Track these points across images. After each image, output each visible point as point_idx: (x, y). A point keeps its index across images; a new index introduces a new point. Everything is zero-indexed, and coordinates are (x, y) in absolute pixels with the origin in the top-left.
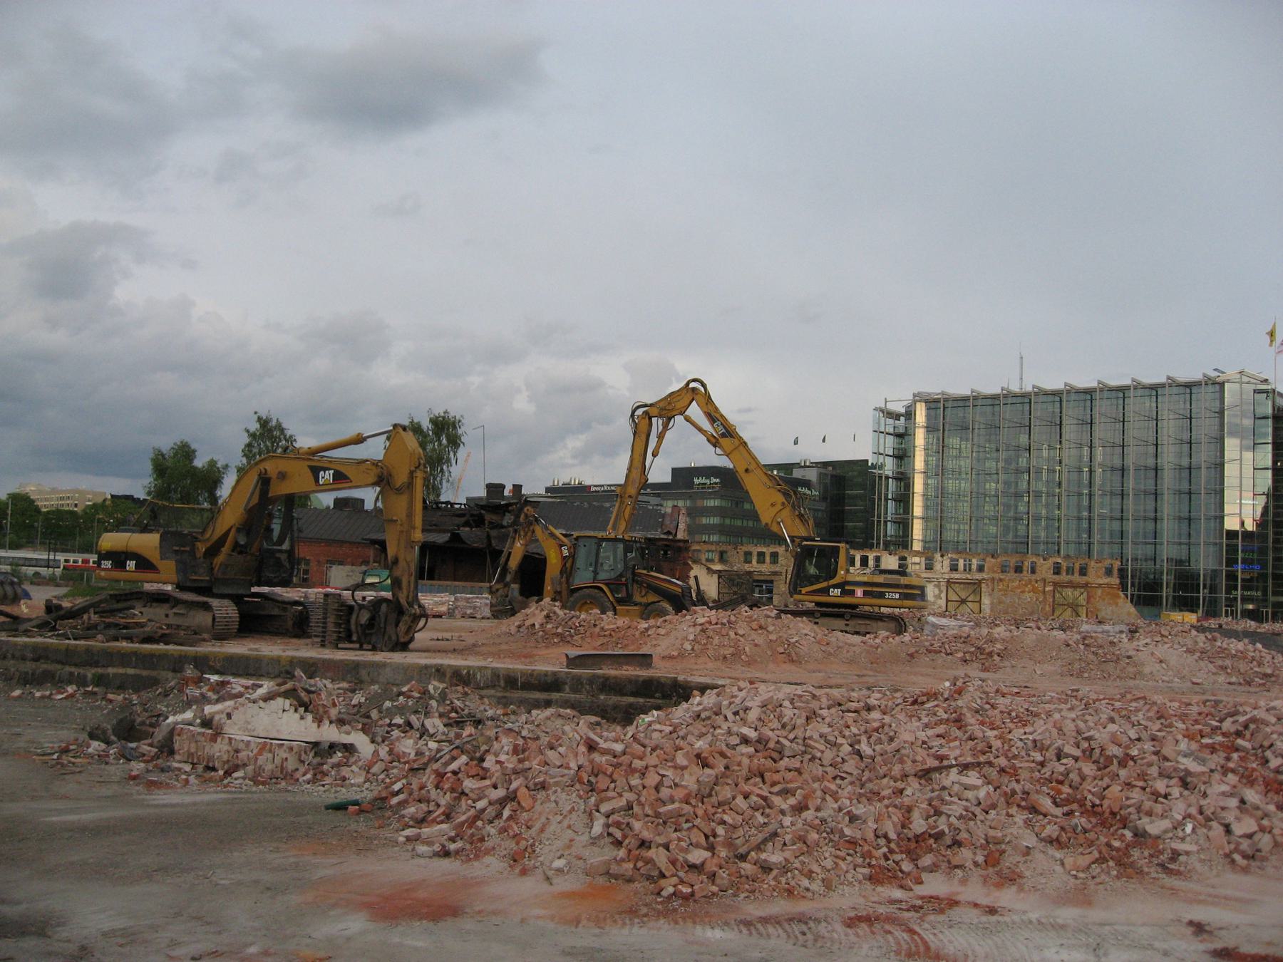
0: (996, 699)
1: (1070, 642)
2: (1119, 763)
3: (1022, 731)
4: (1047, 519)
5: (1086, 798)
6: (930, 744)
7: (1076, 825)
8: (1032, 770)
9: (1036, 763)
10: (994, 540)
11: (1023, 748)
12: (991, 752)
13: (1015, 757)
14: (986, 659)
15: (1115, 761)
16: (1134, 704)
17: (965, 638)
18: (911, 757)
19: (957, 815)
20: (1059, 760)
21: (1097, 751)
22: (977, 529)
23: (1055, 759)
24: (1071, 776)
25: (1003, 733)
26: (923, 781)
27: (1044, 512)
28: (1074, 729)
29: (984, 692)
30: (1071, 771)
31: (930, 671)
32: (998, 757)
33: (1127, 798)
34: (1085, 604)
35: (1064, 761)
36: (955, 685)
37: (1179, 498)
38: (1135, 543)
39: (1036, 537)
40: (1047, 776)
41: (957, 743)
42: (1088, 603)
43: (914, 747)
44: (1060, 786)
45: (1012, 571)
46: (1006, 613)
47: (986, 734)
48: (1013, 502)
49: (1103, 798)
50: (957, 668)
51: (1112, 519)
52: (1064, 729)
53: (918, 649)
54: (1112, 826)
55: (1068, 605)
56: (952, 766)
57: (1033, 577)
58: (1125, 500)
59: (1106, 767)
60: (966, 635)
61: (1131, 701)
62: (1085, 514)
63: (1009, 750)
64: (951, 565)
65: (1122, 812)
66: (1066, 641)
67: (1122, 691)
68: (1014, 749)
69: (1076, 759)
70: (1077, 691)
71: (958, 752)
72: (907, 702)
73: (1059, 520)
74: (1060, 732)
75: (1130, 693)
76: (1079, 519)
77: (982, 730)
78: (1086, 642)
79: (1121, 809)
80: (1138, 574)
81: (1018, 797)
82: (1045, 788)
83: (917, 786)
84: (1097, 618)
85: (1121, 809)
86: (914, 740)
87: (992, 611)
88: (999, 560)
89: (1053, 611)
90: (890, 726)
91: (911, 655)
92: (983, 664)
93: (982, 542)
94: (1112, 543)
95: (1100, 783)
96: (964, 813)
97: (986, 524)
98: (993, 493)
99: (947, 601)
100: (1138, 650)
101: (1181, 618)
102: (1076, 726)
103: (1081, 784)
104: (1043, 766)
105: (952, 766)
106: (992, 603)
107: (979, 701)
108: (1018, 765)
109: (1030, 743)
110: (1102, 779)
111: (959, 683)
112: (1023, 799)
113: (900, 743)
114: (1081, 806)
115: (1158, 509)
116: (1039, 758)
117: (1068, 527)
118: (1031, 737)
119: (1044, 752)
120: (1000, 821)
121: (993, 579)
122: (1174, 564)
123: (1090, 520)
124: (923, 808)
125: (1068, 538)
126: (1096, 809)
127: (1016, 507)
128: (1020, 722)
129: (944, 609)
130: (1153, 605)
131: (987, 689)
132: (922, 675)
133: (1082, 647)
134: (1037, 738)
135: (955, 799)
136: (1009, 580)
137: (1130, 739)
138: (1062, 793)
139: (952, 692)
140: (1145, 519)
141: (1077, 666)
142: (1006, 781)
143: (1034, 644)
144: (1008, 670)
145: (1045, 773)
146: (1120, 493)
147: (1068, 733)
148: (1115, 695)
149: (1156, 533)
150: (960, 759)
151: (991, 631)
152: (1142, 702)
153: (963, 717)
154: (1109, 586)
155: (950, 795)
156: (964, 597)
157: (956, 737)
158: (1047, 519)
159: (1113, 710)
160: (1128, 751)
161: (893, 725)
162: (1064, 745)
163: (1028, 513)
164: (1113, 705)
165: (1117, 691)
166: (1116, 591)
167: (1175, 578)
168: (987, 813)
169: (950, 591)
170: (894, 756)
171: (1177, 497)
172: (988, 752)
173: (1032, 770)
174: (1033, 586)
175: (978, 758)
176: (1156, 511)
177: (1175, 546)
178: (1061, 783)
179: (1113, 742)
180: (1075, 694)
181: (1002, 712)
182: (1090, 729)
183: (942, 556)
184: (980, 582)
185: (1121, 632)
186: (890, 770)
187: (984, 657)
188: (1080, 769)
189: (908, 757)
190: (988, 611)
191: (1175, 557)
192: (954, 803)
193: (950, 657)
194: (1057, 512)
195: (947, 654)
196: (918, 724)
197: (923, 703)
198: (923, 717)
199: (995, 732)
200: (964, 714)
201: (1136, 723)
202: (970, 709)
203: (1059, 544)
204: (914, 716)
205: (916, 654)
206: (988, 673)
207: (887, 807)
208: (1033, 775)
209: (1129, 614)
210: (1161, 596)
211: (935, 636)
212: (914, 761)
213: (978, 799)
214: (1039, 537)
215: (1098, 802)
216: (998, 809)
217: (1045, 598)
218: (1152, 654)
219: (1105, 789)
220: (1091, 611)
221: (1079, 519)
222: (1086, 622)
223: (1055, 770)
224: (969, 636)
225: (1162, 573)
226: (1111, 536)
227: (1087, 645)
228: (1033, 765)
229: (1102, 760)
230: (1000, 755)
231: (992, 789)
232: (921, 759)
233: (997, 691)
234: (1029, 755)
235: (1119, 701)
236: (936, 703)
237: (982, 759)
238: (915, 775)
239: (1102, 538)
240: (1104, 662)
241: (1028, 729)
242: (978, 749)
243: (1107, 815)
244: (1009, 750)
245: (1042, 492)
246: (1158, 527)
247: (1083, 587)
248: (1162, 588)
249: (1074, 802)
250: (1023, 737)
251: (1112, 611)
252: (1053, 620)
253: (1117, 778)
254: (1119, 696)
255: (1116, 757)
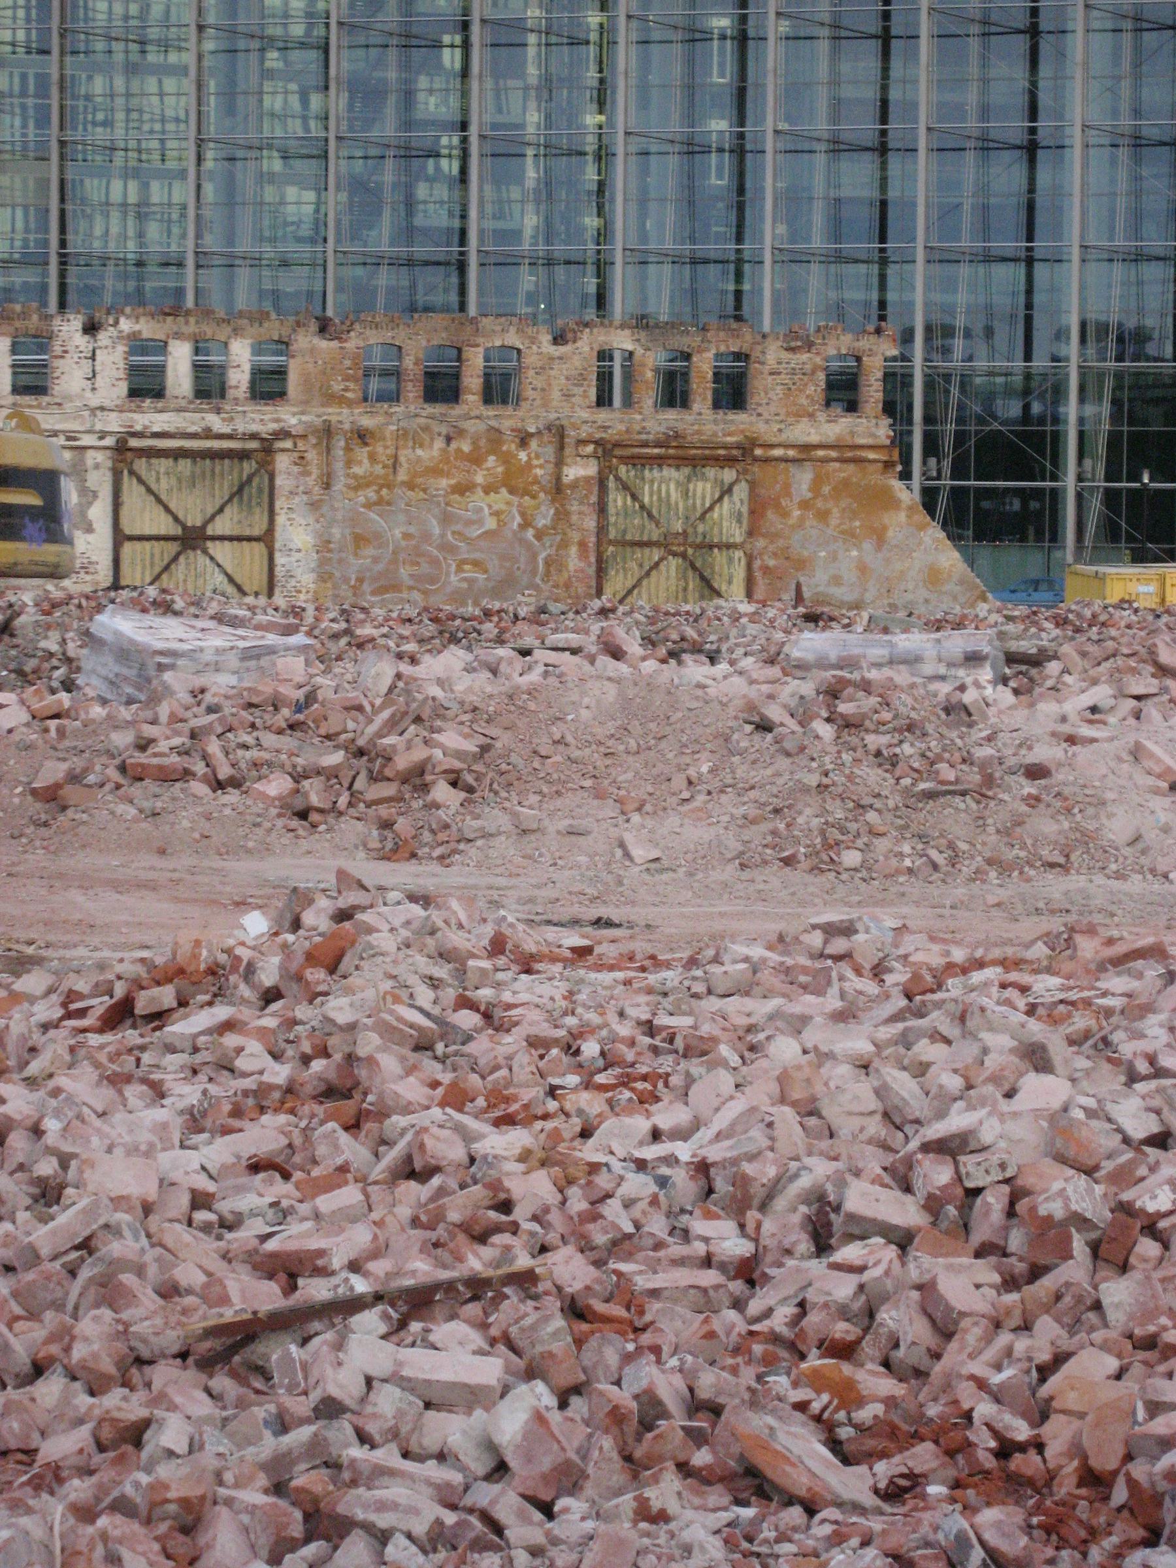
0: (498, 985)
1: (774, 713)
2: (1095, 1248)
3: (641, 1124)
4: (550, 150)
5: (968, 1416)
6: (225, 1207)
7: (962, 1541)
8: (705, 1303)
9: (723, 1267)
10: (30, 276)
11: (654, 1202)
12: (514, 1229)
13: (621, 1245)
14: (399, 799)
15: (1079, 1245)
16: (1117, 983)
17: (299, 708)
18: (152, 1271)
19: (420, 1528)
20: (822, 1246)
21: (994, 1201)
22: (230, 200)
23: (805, 1245)
24: (887, 1316)
25: (556, 1136)
26: (222, 1382)
27: (533, 118)
28: (873, 1104)
29: (444, 955)
30: (885, 1298)
31: (144, 864)
32: (544, 1249)
33: (1155, 1408)
34: (738, 539)
35: (850, 1253)
36: (296, 925)
37: (1137, 49)
38: (939, 258)
39: (504, 236)
40: (779, 1322)
41: (349, 1195)
42: (750, 533)
43: (154, 1221)
44: (847, 1369)
45: (413, 391)
46: (388, 586)
47: (479, 1147)
48: (392, 75)
49: (1042, 1414)
50: (267, 849)
51: (838, 147)
52: (830, 1111)
53: (78, 763)
54: (1093, 1534)
55: (665, 544)
56: (353, 1305)
57: (507, 419)
58: (896, 64)
59: (1036, 1272)
60: (300, 694)
61: (1102, 967)
62: (719, 126)
63: (595, 1217)
64: (134, 371)
65: (1139, 1470)
66: (751, 707)
67: (1056, 924)
68: (612, 1210)
69: (903, 1241)
70: (847, 930)
71: (360, 1237)
72: (82, 1013)
73: (603, 155)
74: (812, 1121)
75: (1091, 931)
76: (693, 149)
77: (459, 1129)
78: (843, 708)
79: (1129, 1457)
80: (955, 391)
81: (675, 1424)
82: (780, 1382)
83: (203, 1407)
84: (799, 599)
85: (1129, 1457)
86: (151, 1191)
87: (323, 577)
88: (353, 343)
89: (601, 571)
90: (37, 1131)
91: (51, 796)
92: (387, 825)
93: (256, 262)
94: (839, 258)
95: (1021, 1345)
96: (450, 1518)
97: (272, 178)
98: (297, 30)
99: (120, 538)
100: (1071, 740)
101: (1151, 588)
102: (881, 1092)
103: (937, 1356)
104: (751, 1283)
105: (353, 1305)
106: (324, 545)
107: (425, 996)
108: (643, 1282)
109: (680, 1177)
110: (1026, 1327)
111: (317, 918)
112: (697, 1438)
113: (90, 1212)
114: (951, 1453)
115: (1044, 99)
116: (735, 1246)
117: (644, 190)
118: (684, 1151)
119: (752, 1216)
120: (620, 1543)
121: (327, 432)
122: (1112, 347)
123: (740, 150)
124: (252, 1510)
125: (644, 237)
126: (1017, 1462)
127: (408, 96)
128: (625, 1082)
129: (104, 575)
130: (1023, 539)
131: (456, 940)
132: (117, 886)
133: (826, 731)
134: (714, 1154)
135: (388, 1455)
136: (403, 435)
137: (1126, 1140)
138: (861, 1402)
139: (299, 958)
140: (987, 146)
141: (808, 817)
142: (612, 1357)
143: (611, 728)
144: (503, 846)
145: (768, 1313)
146: (875, 27)
147: (846, 1127)
148: (1029, 945)
149: (1031, 207)
150: (379, 1267)
151: (405, 668)
152: (1152, 971)
153: (362, 1073)
154: (848, 453)
155: (363, 1438)
156: (194, 519)
157: (343, 1169)
158: (550, 150)
159: (1031, 1010)
160: (1126, 1196)
161: (52, 1125)
162: (841, 1184)
163: (464, 126)
164: (1024, 989)
165: (1029, 927)
166: (875, 476)
167: (1115, 418)
168: (548, 1510)
169: (132, 493)
170: (73, 1273)
171: (1127, 39)
172: (498, 1229)
173: (705, 1303)
174: (507, 459)
175: (460, 1259)
176: (1033, 112)
177: (1118, 269)
178: (844, 1351)
179: (1061, 1159)
180: (839, 945)
181: (536, 1043)
182: (943, 1103)
183: (91, 328)
184: (267, 447)
185: (973, 659)
186: (65, 1337)
187: (388, 790)
188: (926, 1288)
189: (140, 1271)
190: (306, 579)
191: (1114, 319)
192: (391, 1473)
193: (232, 796)
194: (592, 119)
195: (219, 785)
196: (159, 1114)
197: (159, 1018)
198: (170, 1080)
199: (518, 1138)
200: (371, 1061)
201: (1142, 1067)
202: (389, 1032)
203: (602, 267)
204: (128, 1079)
205: (70, 793)
206: (411, 867)
207: (85, 1513)
208: (716, 1325)
209: (934, 577)
210: (1056, 496)
211: (154, 700)
212: (169, 1291)
213: (490, 1446)
214: (515, 235)
215: (1021, 1431)
216: (589, 1490)
217: (562, 515)
218: (1137, 753)
219: (1045, 1372)
220: (766, 570)
221: (693, 149)
222: (754, 618)
223: (811, 1295)
224: (311, 698)
225: (1058, 392)
226: (836, 231)
227: (849, 725)
228: (710, 1278)
229: (1016, 1240)
230: (552, 1238)
231: (549, 1400)
232: (201, 1278)
233: (497, 946)
234: (686, 1235)
235: (1049, 970)
236: (222, 1012)
237: (477, 1261)
238: (183, 1355)
239: (793, 237)
240: (930, 795)
241: (668, 1115)
242: (454, 1216)
243: (1066, 1486)
244: (595, 1217)
245: (519, 25)
246: (1044, 177)
247: (730, 461)
248: (1057, 458)
249: (918, 1437)
250: (650, 1152)
251: (863, 569)
252: (604, 612)
253: (1092, 1316)
254: (1039, 951)
255: (1080, 1221)
